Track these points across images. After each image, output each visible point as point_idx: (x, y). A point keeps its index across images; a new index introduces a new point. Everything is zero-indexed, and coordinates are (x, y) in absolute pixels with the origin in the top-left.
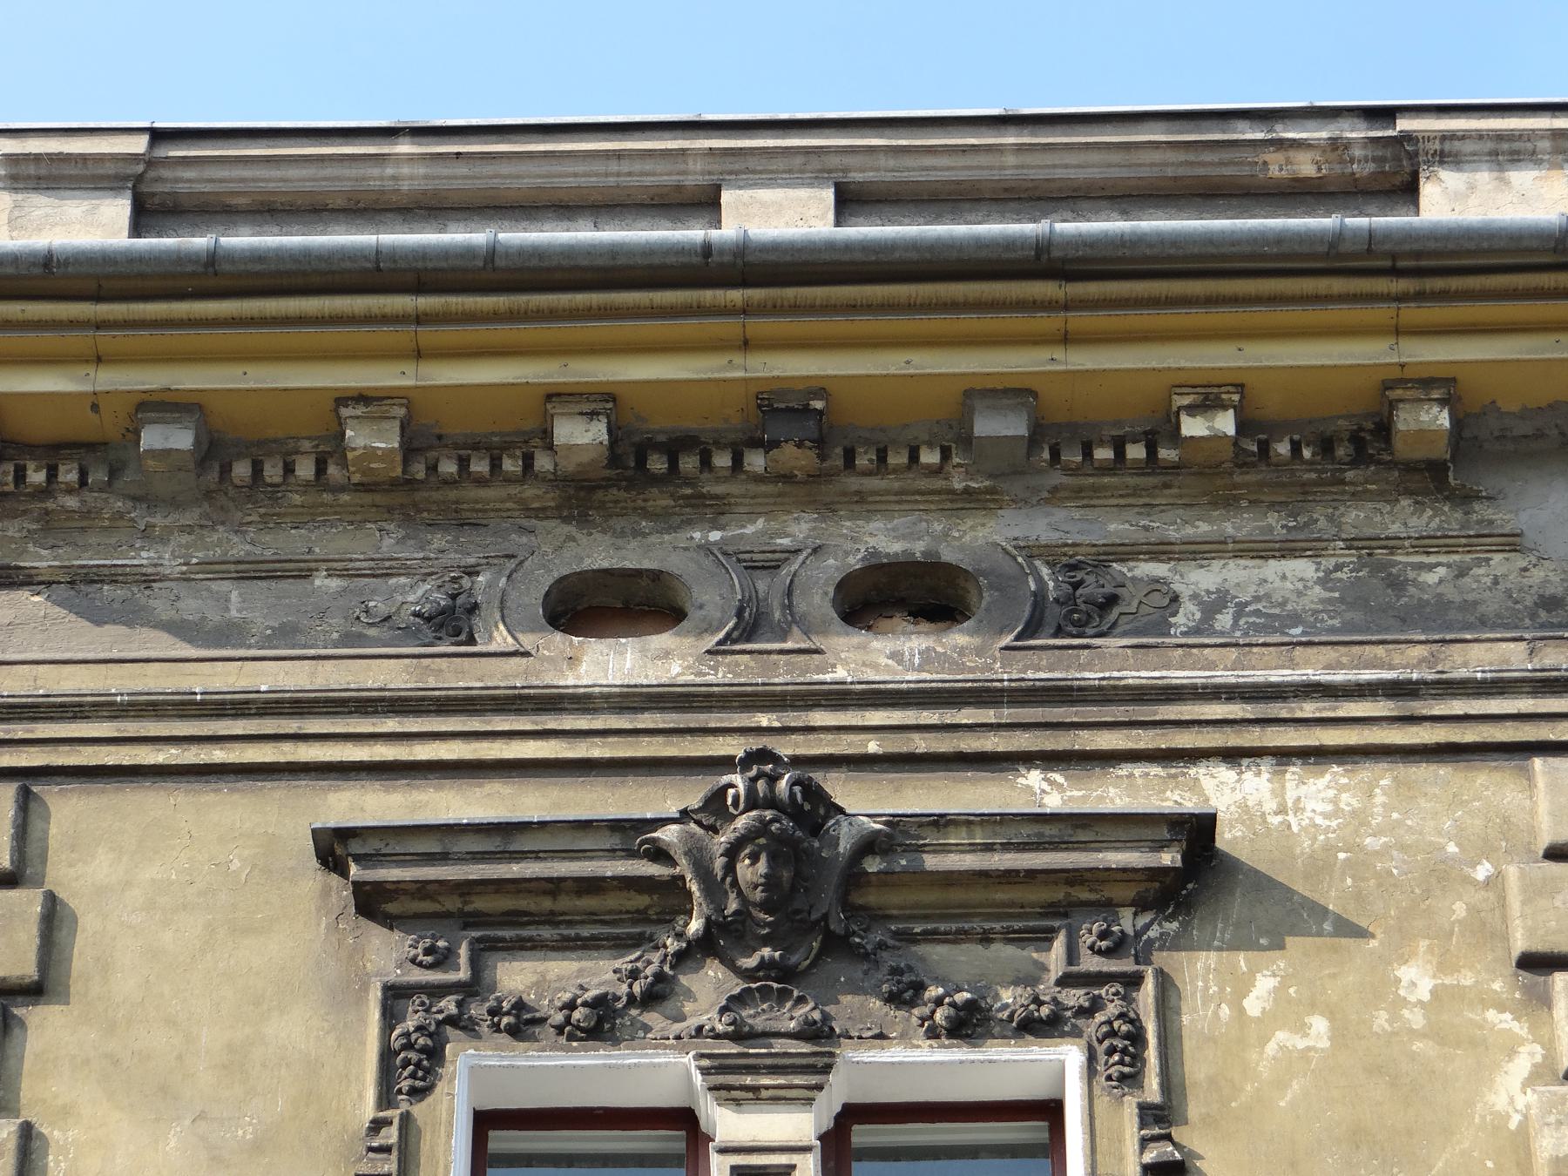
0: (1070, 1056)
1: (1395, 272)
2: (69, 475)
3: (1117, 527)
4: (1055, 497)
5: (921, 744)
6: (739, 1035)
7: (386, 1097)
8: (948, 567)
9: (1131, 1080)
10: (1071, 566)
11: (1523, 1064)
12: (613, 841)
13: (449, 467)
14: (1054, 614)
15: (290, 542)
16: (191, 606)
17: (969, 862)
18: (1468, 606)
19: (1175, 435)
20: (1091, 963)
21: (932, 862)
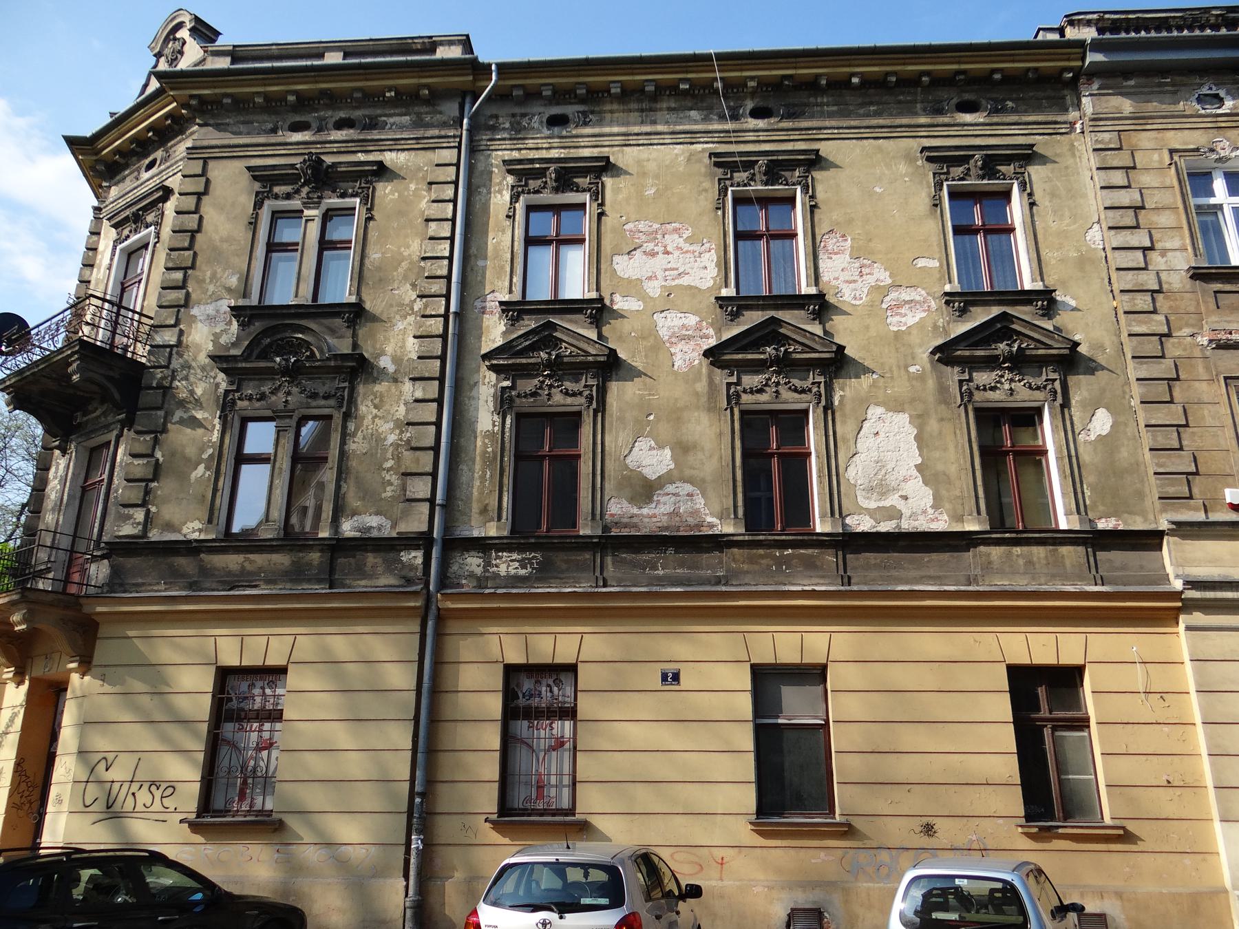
0: (358, 200)
1: (418, 67)
2: (214, 107)
3: (379, 112)
4: (370, 107)
5: (342, 149)
6: (309, 198)
7: (254, 210)
8: (353, 120)
9: (367, 204)
10: (371, 118)
12: (289, 167)
13: (274, 104)
14: (993, 110)
15: (251, 117)
16: (235, 129)
18: (432, 124)
19: (384, 96)
20: (363, 185)
21: (339, 169)
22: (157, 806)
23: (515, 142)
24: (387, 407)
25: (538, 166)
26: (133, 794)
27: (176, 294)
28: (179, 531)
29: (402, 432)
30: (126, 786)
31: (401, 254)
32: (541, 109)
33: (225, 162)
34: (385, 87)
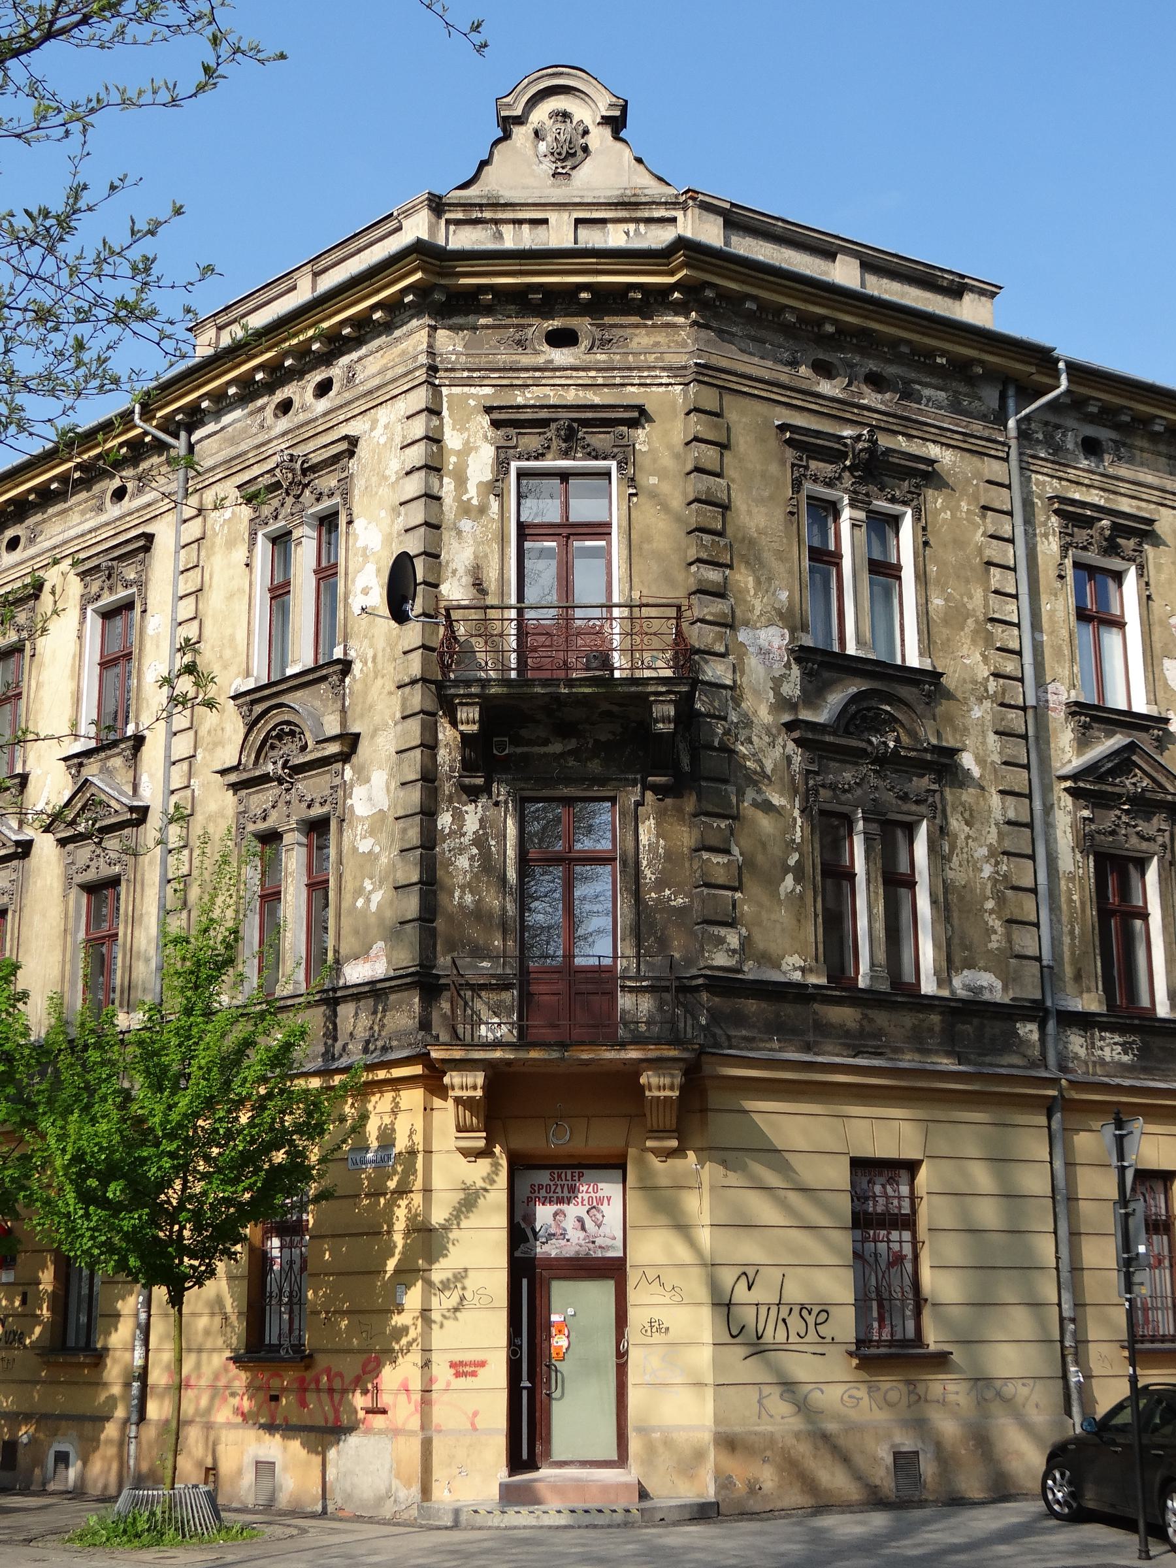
3: (913, 375)
11: (981, 531)
15: (762, 334)
17: (897, 461)
20: (913, 489)
21: (891, 459)
22: (812, 1337)
23: (1057, 467)
24: (977, 825)
25: (1089, 513)
26: (784, 1320)
27: (720, 606)
28: (777, 966)
29: (997, 864)
30: (774, 1309)
31: (964, 605)
32: (1075, 425)
33: (747, 401)
34: (939, 349)
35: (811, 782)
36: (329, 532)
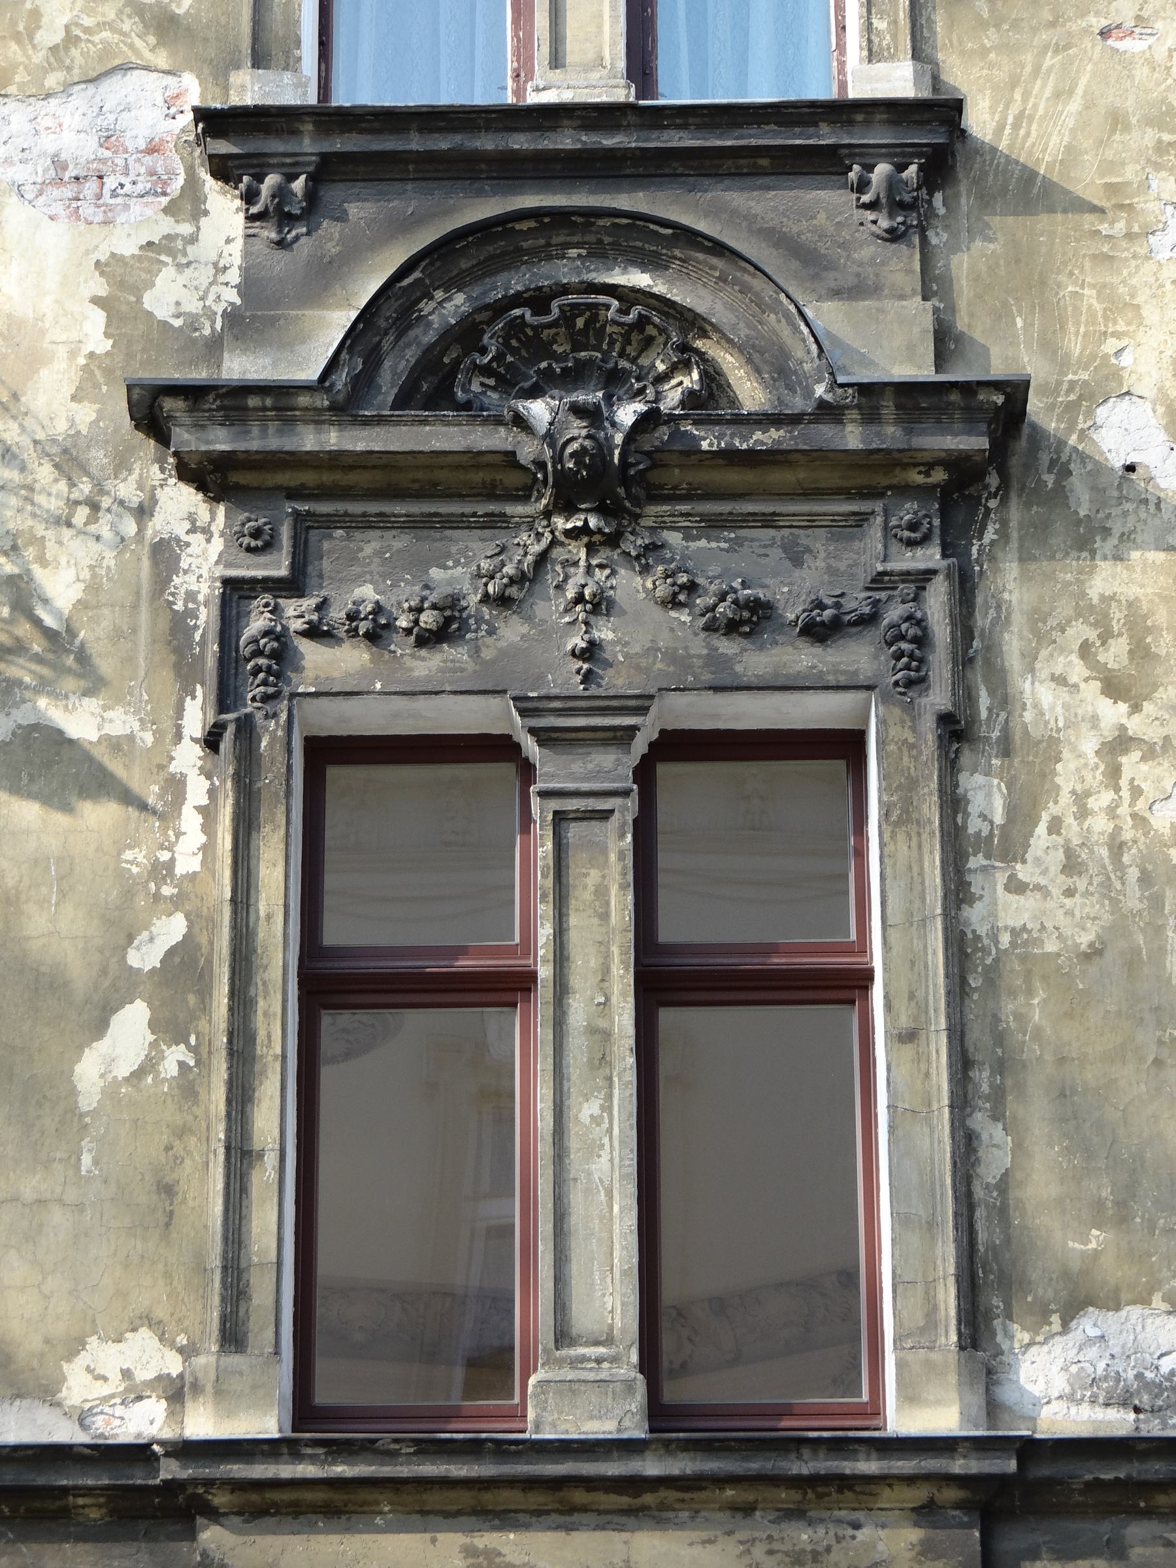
35: (257, 623)
36: (968, 607)
